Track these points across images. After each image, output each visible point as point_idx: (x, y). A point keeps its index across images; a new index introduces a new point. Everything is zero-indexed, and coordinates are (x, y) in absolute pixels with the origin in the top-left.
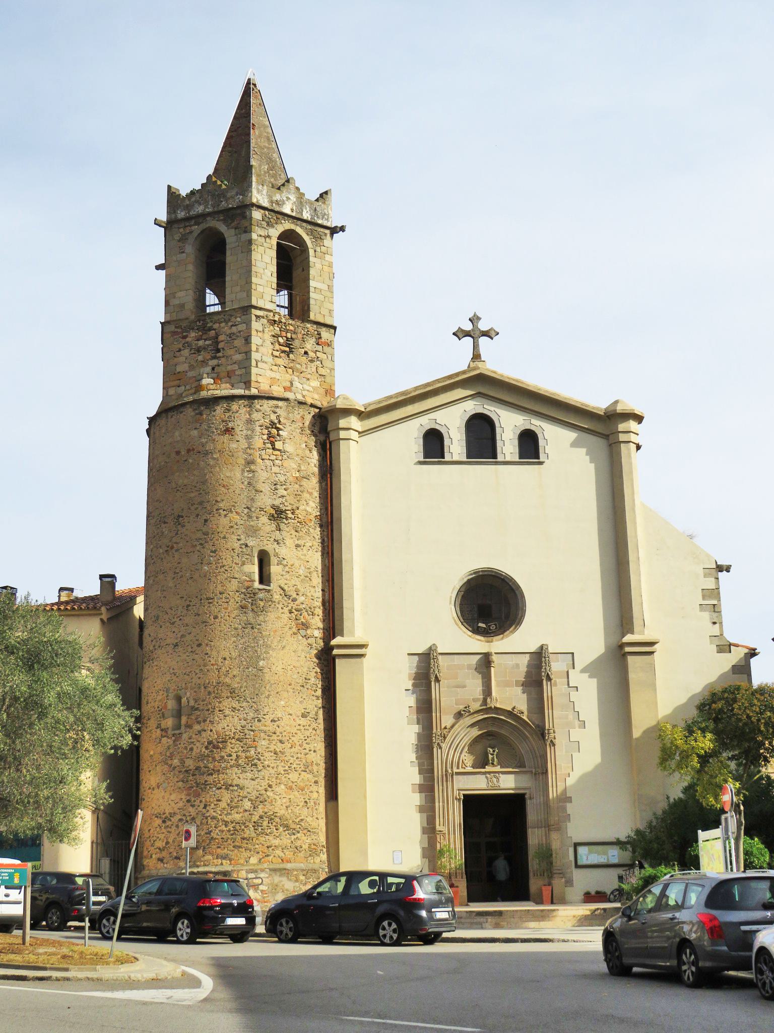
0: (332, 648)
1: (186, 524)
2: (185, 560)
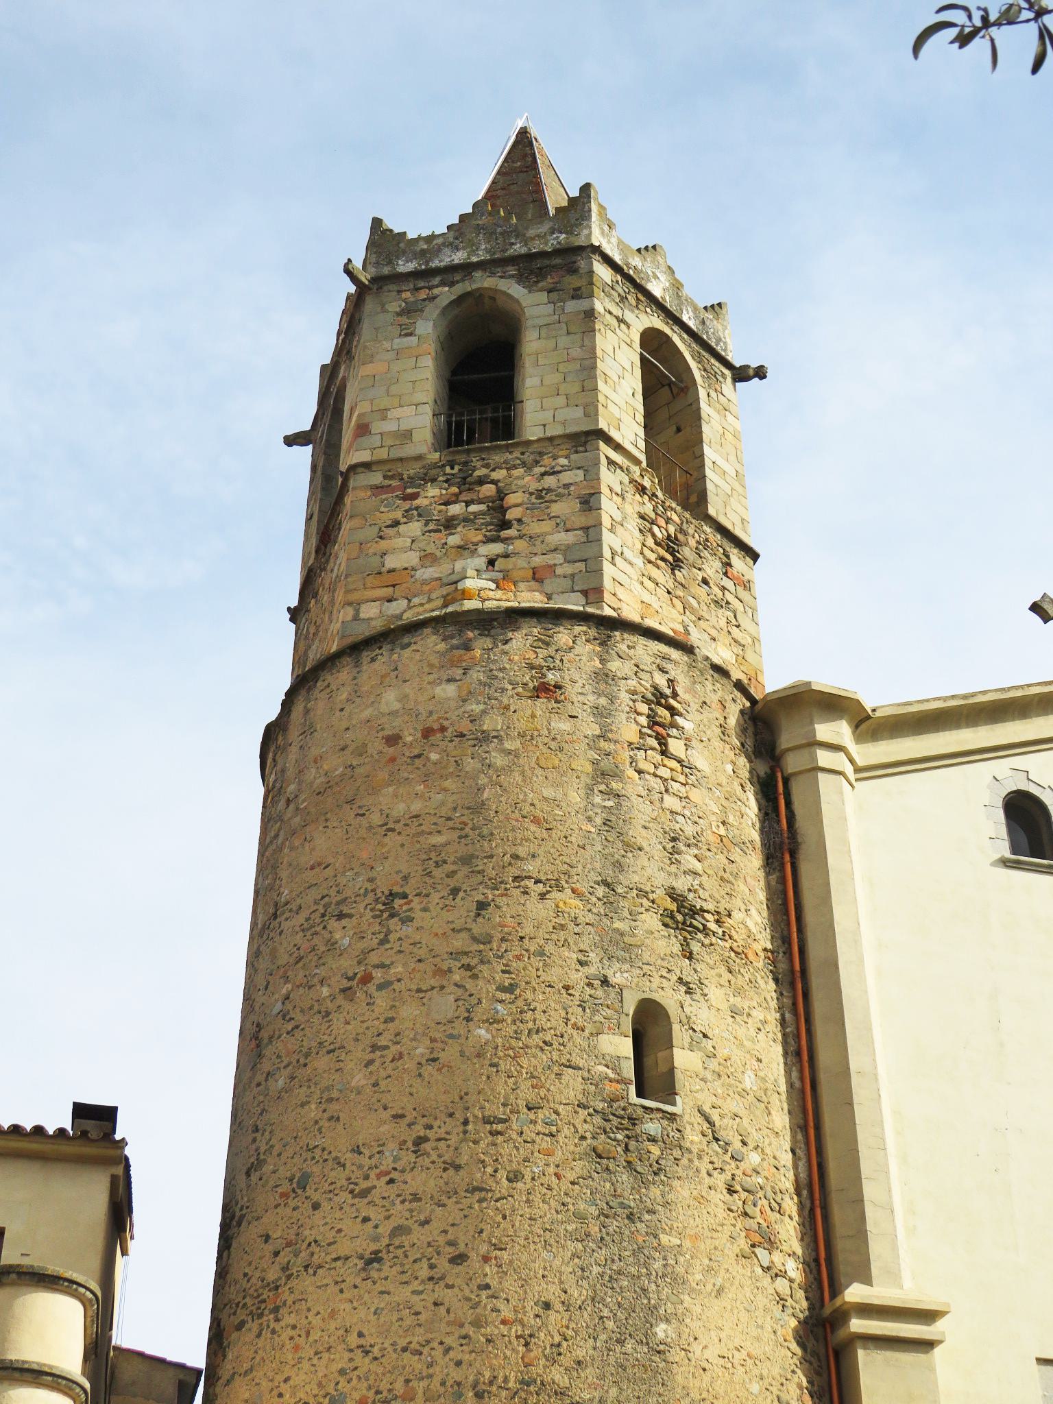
0: (842, 1316)
1: (418, 914)
2: (409, 1011)
